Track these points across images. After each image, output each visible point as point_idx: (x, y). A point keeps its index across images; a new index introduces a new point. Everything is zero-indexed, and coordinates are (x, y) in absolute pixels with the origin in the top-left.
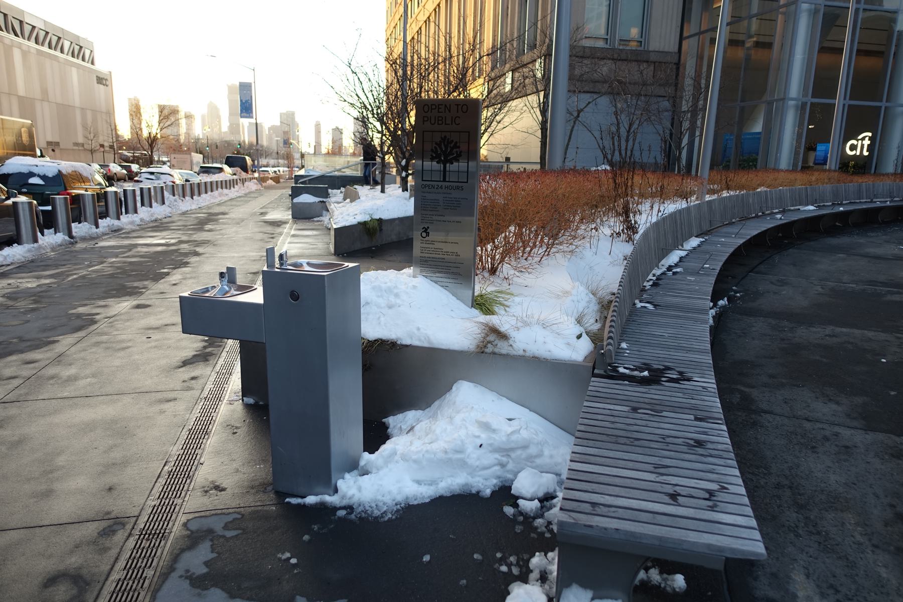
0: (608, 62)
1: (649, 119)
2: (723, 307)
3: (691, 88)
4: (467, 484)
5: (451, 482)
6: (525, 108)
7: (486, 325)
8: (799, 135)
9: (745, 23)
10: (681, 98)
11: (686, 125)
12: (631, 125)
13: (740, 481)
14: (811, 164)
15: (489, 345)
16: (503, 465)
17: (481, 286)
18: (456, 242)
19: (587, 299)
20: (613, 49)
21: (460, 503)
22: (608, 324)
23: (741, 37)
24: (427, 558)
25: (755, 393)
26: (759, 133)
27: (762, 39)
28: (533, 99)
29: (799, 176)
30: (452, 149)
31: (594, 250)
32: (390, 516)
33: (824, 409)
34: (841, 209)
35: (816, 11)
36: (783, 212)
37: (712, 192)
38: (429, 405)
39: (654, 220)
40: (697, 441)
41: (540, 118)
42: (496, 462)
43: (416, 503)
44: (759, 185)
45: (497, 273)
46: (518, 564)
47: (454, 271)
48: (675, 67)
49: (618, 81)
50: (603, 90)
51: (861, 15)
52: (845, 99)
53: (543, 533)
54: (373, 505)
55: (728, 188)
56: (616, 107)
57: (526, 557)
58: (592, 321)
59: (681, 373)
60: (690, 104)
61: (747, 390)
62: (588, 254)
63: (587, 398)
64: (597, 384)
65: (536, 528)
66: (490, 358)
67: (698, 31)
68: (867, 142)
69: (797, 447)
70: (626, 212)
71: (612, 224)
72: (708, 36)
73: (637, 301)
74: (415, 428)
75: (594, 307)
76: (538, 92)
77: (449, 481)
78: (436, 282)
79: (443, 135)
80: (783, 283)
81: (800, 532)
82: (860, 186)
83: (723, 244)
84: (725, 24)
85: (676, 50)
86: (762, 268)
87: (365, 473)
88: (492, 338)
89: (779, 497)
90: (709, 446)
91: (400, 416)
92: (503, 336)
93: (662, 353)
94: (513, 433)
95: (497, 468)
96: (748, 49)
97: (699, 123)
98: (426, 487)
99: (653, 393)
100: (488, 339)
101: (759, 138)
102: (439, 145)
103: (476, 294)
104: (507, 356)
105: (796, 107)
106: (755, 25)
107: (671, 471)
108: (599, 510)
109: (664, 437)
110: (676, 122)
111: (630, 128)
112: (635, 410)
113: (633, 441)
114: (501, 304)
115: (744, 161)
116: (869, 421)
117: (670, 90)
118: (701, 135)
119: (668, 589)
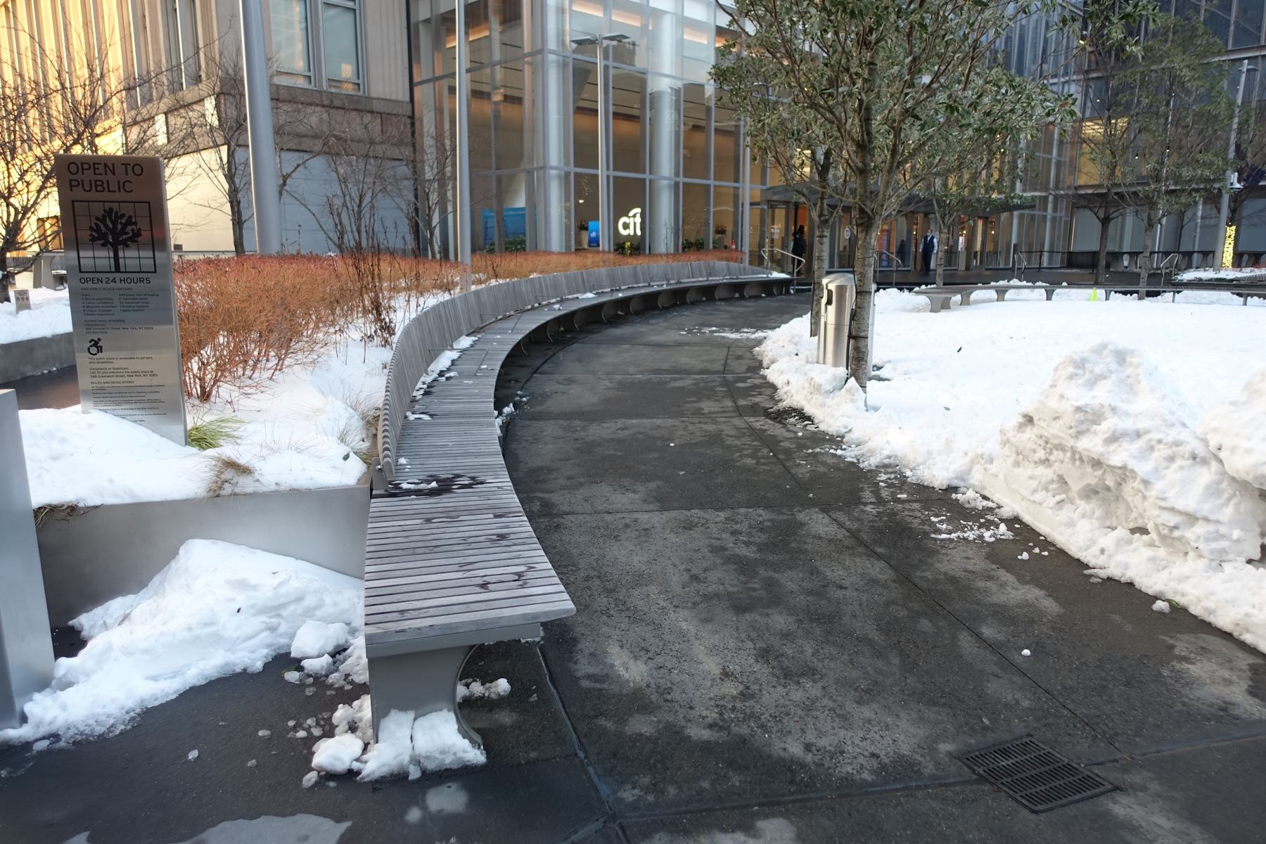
0: (318, 109)
1: (384, 190)
2: (510, 415)
3: (434, 150)
4: (227, 664)
5: (204, 666)
6: (200, 171)
7: (219, 459)
8: (567, 210)
9: (488, 70)
10: (423, 162)
11: (434, 197)
12: (361, 197)
13: (546, 559)
14: (586, 246)
15: (226, 485)
16: (272, 629)
17: (196, 416)
18: (153, 359)
19: (347, 415)
20: (320, 92)
21: (227, 687)
22: (380, 440)
23: (486, 88)
24: (193, 755)
25: (554, 498)
26: (523, 209)
27: (510, 92)
28: (210, 157)
29: (574, 259)
30: (125, 226)
31: (343, 359)
32: (123, 727)
33: (621, 500)
34: (620, 295)
35: (565, 65)
36: (561, 301)
37: (480, 282)
38: (146, 586)
39: (413, 316)
40: (498, 535)
41: (226, 186)
42: (263, 626)
43: (157, 703)
44: (532, 272)
45: (212, 399)
46: (318, 724)
47: (153, 401)
48: (409, 121)
49: (336, 137)
50: (317, 148)
51: (611, 71)
52: (608, 169)
53: (342, 688)
54: (91, 722)
55: (496, 276)
56: (337, 172)
57: (325, 715)
58: (358, 438)
59: (473, 478)
60: (435, 171)
61: (546, 496)
62: (336, 363)
63: (368, 537)
64: (377, 505)
65: (332, 685)
66: (230, 502)
67: (431, 76)
68: (638, 219)
69: (601, 540)
70: (377, 307)
71: (359, 327)
72: (445, 84)
73: (409, 414)
74: (133, 614)
75: (357, 423)
76: (216, 146)
77: (201, 665)
78: (123, 417)
79: (107, 206)
80: (570, 382)
81: (612, 612)
82: (635, 269)
83: (499, 342)
84: (464, 71)
85: (407, 98)
86: (546, 367)
87: (66, 685)
88: (228, 474)
89: (589, 588)
90: (512, 536)
91: (98, 611)
92: (244, 470)
93: (448, 462)
94: (280, 584)
95: (266, 634)
96: (496, 103)
97: (449, 194)
98: (168, 681)
99: (445, 501)
100: (224, 477)
101: (523, 216)
102: (103, 220)
103: (189, 427)
104: (253, 495)
105: (559, 177)
106: (499, 73)
107: (477, 565)
108: (407, 615)
109: (465, 539)
110: (419, 193)
111: (361, 202)
112: (428, 521)
113: (433, 549)
114: (228, 436)
115: (511, 243)
116: (663, 502)
117: (407, 152)
118: (455, 211)
119: (493, 696)
